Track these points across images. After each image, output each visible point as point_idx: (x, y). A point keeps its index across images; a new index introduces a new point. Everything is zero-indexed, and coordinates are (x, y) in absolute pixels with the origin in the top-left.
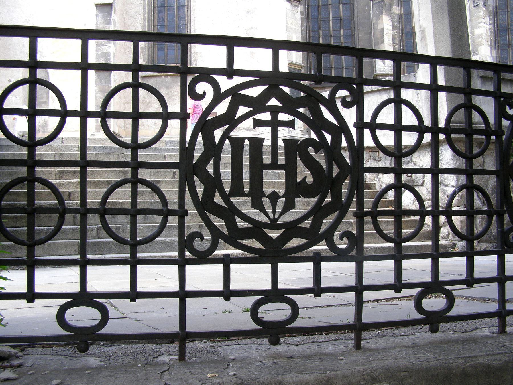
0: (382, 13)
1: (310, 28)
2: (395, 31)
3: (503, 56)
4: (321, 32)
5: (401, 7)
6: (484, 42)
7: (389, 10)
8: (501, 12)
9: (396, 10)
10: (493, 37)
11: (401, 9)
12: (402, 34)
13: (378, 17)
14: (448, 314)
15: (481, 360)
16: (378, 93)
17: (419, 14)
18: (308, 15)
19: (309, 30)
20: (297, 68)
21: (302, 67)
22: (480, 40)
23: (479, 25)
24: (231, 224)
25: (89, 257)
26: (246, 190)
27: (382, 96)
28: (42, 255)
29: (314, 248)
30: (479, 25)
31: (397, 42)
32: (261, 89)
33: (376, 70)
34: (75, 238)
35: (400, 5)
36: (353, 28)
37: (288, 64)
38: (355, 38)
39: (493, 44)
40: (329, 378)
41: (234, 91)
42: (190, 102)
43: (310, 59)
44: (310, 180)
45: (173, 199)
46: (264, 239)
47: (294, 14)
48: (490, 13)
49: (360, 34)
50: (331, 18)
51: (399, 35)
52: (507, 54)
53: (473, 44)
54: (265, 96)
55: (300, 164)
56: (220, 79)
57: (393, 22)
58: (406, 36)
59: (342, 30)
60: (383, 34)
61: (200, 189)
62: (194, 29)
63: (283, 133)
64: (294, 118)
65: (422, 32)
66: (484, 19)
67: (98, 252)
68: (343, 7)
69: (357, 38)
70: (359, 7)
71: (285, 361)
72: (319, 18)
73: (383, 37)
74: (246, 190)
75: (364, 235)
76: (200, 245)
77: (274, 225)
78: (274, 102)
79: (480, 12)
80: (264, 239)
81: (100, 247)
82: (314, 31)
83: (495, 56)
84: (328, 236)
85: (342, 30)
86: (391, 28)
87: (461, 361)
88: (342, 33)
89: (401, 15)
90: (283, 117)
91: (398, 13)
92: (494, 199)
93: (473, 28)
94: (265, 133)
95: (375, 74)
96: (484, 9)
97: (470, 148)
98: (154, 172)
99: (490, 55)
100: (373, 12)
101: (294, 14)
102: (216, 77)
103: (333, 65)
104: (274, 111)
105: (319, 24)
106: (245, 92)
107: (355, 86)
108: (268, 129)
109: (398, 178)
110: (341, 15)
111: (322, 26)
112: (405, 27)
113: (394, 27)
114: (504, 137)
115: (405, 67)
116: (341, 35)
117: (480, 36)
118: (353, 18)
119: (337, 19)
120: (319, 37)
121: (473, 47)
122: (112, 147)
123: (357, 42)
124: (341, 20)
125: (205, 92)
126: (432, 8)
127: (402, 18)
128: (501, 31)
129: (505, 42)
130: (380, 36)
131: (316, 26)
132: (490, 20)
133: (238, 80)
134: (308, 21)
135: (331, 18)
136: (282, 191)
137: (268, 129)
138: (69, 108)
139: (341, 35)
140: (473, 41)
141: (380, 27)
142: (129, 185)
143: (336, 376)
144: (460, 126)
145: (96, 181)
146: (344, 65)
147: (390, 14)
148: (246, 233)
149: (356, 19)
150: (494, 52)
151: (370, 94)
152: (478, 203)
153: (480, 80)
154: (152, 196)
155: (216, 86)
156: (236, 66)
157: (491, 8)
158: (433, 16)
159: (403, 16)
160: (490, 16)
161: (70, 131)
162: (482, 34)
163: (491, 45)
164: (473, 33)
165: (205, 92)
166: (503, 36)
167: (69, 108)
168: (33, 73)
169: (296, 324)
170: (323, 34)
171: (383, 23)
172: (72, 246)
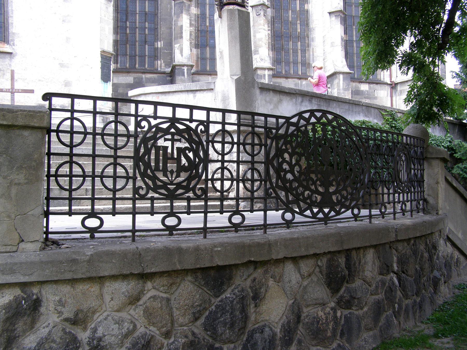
0: (182, 12)
1: (119, 19)
2: (192, 28)
3: (277, 57)
4: (128, 23)
5: (198, 8)
6: (264, 45)
7: (188, 10)
8: (277, 21)
9: (194, 10)
10: (270, 41)
11: (198, 10)
12: (198, 31)
13: (179, 15)
15: (256, 241)
16: (186, 93)
17: (219, 40)
18: (117, 7)
19: (117, 21)
20: (109, 55)
21: (112, 54)
22: (261, 42)
23: (260, 31)
24: (154, 183)
25: (96, 197)
26: (161, 169)
27: (189, 95)
29: (187, 195)
30: (260, 31)
31: (193, 37)
32: (168, 124)
33: (174, 61)
35: (197, 6)
36: (156, 23)
37: (101, 51)
38: (157, 30)
39: (270, 46)
40: (198, 245)
41: (157, 126)
42: (139, 130)
43: (117, 47)
44: (187, 165)
45: (131, 171)
46: (168, 190)
47: (107, 8)
48: (268, 21)
49: (162, 28)
50: (138, 12)
51: (195, 32)
52: (281, 55)
53: (254, 45)
54: (169, 128)
55: (183, 158)
56: (151, 120)
57: (190, 20)
58: (201, 33)
59: (147, 23)
60: (182, 30)
61: (142, 168)
62: (12, 10)
63: (177, 145)
64: (180, 138)
65: (221, 53)
66: (264, 26)
68: (148, 3)
69: (159, 31)
70: (162, 4)
71: (178, 242)
72: (127, 11)
73: (182, 33)
74: (161, 169)
76: (142, 192)
77: (172, 183)
78: (173, 130)
79: (261, 20)
80: (168, 190)
81: (101, 193)
82: (122, 22)
83: (272, 56)
84: (193, 189)
85: (147, 23)
86: (189, 25)
87: (249, 241)
88: (147, 26)
89: (198, 15)
90: (176, 137)
91: (195, 13)
92: (263, 175)
93: (255, 32)
94: (168, 144)
95: (174, 64)
96: (264, 18)
97: (253, 150)
99: (268, 56)
100: (174, 10)
101: (107, 8)
102: (149, 119)
103: (137, 54)
104: (173, 134)
105: (127, 16)
106: (160, 126)
107: (206, 124)
108: (170, 142)
109: (223, 164)
110: (147, 10)
111: (130, 18)
112: (201, 25)
113: (191, 25)
114: (268, 147)
115: (199, 60)
116: (146, 28)
117: (260, 40)
118: (156, 13)
119: (143, 13)
120: (127, 27)
121: (254, 47)
123: (159, 34)
124: (146, 14)
125: (145, 126)
126: (228, 37)
127: (198, 17)
128: (276, 37)
129: (280, 46)
130: (180, 31)
131: (124, 18)
132: (268, 27)
133: (159, 121)
134: (118, 13)
135: (138, 12)
136: (175, 170)
137: (170, 142)
139: (146, 28)
140: (255, 42)
141: (179, 24)
142: (112, 166)
143: (201, 245)
144: (244, 122)
146: (147, 54)
147: (189, 14)
148: (161, 187)
149: (159, 15)
150: (271, 53)
151: (180, 93)
152: (256, 176)
153: (259, 90)
155: (149, 123)
156: (158, 115)
157: (269, 18)
158: (229, 43)
159: (199, 16)
160: (268, 24)
162: (262, 39)
163: (269, 47)
164: (255, 36)
165: (145, 126)
166: (278, 41)
168: (72, 115)
169: (180, 227)
170: (129, 24)
171: (182, 21)
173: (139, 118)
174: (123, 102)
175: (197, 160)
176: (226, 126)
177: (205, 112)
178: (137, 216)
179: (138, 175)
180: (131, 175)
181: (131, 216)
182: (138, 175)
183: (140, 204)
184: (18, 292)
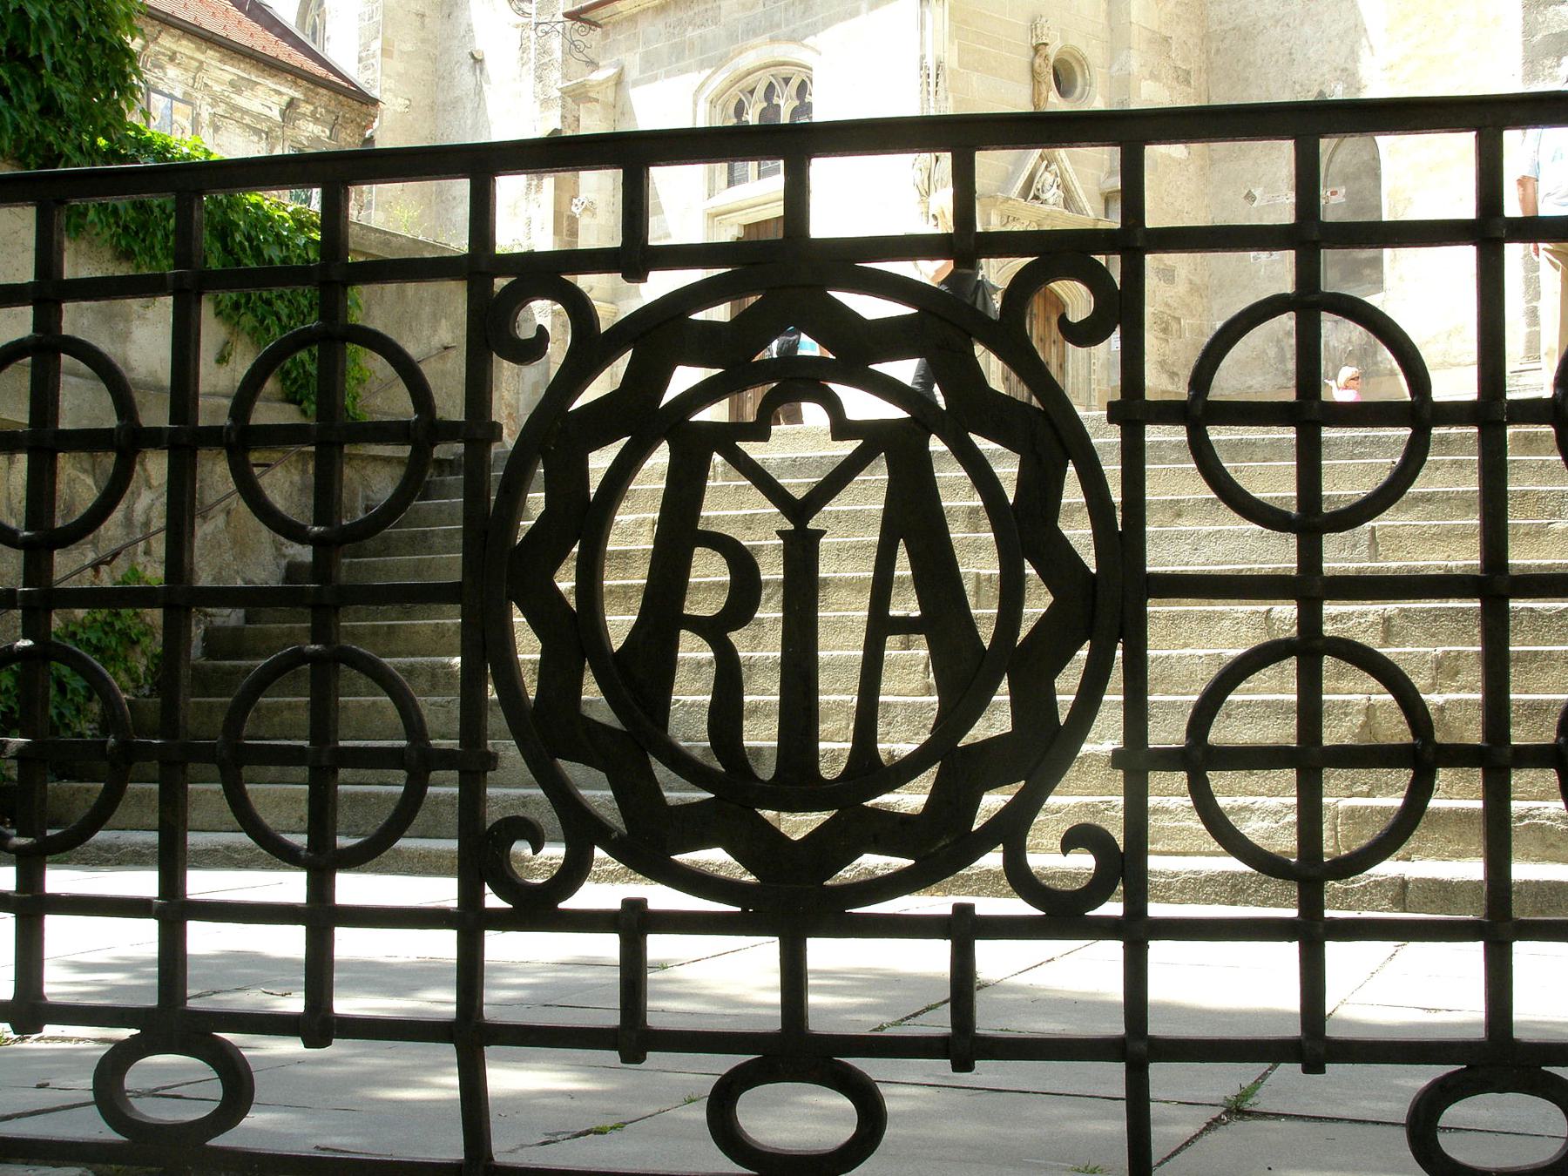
14: (215, 1142)
28: (216, 828)
34: (358, 779)
61: (1073, 492)
67: (363, 829)
75: (1424, 819)
98: (851, 547)
122: (821, 457)
138: (1287, 285)
145: (617, 586)
154: (754, 637)
161: (1459, 365)
167: (1287, 285)
172: (294, 805)
173: (1114, 266)
174: (421, 180)
175: (536, 501)
176: (1518, 388)
177: (1462, 145)
178: (1336, 952)
179: (1106, 439)
180: (1163, 437)
181: (1473, 953)
182: (1106, 439)
183: (1183, 694)
184: (236, 78)
